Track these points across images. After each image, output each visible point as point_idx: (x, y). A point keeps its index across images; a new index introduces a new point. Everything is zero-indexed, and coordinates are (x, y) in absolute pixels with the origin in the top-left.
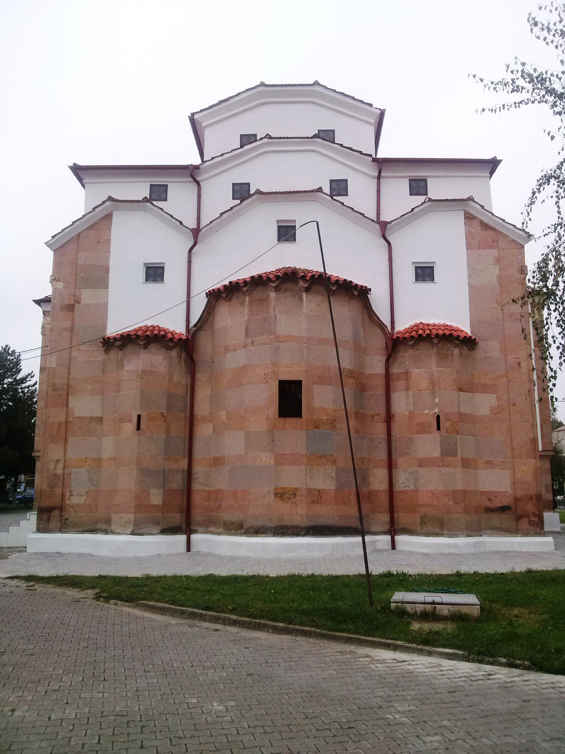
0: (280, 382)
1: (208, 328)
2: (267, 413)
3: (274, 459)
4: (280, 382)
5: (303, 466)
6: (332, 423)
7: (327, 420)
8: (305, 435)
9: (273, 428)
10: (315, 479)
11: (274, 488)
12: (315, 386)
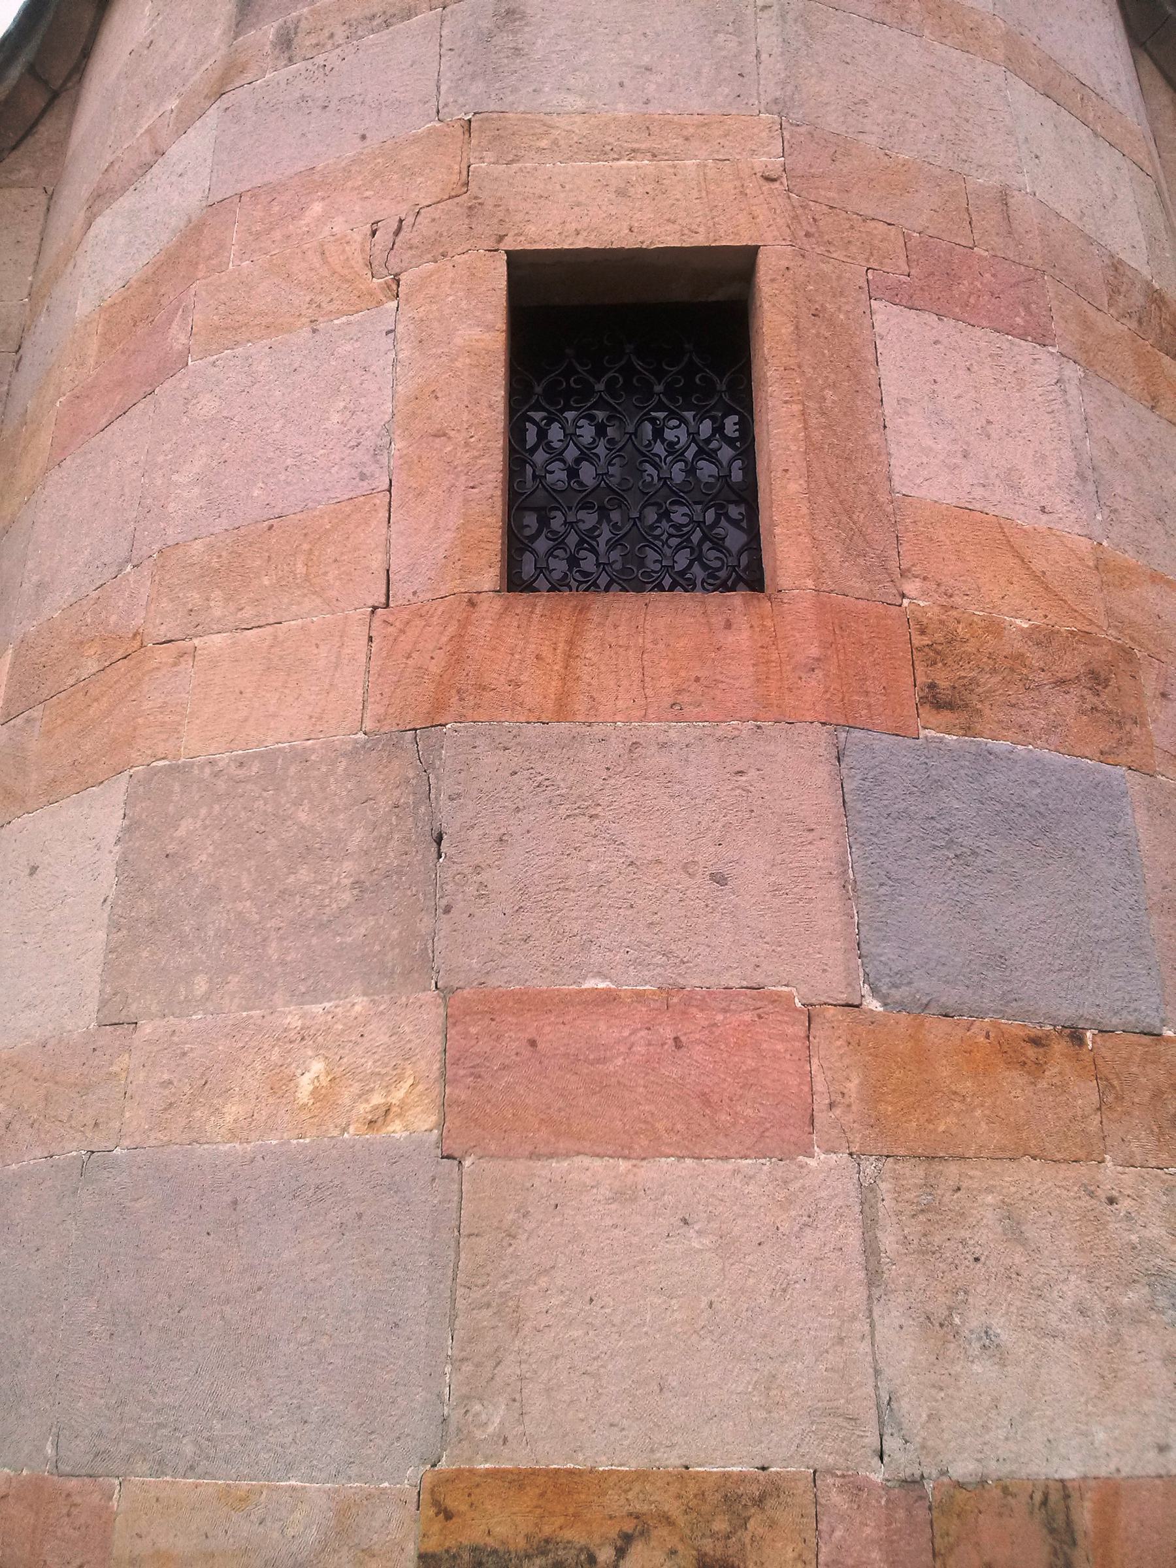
0: (516, 261)
1: (27, 172)
2: (376, 562)
3: (428, 1063)
4: (516, 261)
5: (818, 1161)
6: (1097, 679)
7: (1043, 638)
8: (822, 774)
9: (439, 706)
10: (990, 1345)
11: (413, 1474)
12: (885, 315)
